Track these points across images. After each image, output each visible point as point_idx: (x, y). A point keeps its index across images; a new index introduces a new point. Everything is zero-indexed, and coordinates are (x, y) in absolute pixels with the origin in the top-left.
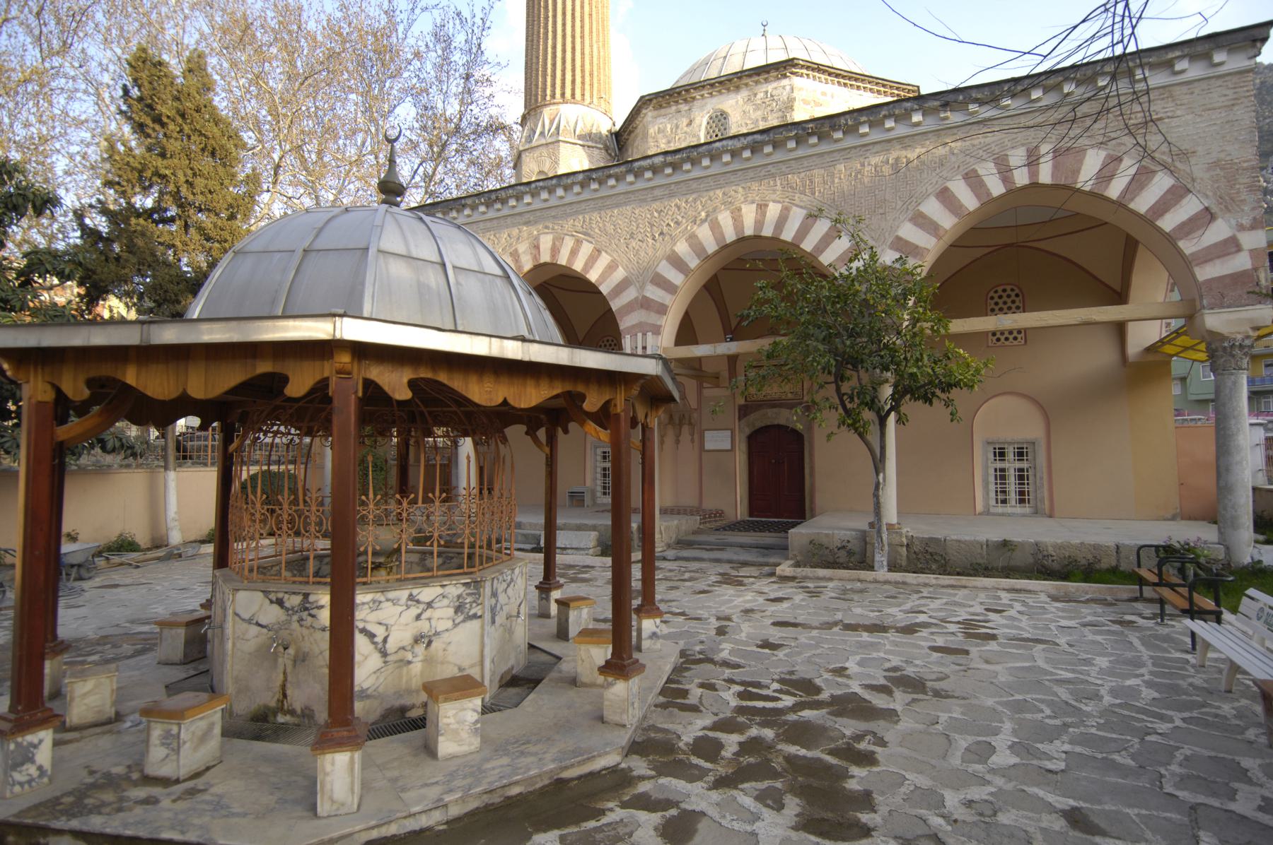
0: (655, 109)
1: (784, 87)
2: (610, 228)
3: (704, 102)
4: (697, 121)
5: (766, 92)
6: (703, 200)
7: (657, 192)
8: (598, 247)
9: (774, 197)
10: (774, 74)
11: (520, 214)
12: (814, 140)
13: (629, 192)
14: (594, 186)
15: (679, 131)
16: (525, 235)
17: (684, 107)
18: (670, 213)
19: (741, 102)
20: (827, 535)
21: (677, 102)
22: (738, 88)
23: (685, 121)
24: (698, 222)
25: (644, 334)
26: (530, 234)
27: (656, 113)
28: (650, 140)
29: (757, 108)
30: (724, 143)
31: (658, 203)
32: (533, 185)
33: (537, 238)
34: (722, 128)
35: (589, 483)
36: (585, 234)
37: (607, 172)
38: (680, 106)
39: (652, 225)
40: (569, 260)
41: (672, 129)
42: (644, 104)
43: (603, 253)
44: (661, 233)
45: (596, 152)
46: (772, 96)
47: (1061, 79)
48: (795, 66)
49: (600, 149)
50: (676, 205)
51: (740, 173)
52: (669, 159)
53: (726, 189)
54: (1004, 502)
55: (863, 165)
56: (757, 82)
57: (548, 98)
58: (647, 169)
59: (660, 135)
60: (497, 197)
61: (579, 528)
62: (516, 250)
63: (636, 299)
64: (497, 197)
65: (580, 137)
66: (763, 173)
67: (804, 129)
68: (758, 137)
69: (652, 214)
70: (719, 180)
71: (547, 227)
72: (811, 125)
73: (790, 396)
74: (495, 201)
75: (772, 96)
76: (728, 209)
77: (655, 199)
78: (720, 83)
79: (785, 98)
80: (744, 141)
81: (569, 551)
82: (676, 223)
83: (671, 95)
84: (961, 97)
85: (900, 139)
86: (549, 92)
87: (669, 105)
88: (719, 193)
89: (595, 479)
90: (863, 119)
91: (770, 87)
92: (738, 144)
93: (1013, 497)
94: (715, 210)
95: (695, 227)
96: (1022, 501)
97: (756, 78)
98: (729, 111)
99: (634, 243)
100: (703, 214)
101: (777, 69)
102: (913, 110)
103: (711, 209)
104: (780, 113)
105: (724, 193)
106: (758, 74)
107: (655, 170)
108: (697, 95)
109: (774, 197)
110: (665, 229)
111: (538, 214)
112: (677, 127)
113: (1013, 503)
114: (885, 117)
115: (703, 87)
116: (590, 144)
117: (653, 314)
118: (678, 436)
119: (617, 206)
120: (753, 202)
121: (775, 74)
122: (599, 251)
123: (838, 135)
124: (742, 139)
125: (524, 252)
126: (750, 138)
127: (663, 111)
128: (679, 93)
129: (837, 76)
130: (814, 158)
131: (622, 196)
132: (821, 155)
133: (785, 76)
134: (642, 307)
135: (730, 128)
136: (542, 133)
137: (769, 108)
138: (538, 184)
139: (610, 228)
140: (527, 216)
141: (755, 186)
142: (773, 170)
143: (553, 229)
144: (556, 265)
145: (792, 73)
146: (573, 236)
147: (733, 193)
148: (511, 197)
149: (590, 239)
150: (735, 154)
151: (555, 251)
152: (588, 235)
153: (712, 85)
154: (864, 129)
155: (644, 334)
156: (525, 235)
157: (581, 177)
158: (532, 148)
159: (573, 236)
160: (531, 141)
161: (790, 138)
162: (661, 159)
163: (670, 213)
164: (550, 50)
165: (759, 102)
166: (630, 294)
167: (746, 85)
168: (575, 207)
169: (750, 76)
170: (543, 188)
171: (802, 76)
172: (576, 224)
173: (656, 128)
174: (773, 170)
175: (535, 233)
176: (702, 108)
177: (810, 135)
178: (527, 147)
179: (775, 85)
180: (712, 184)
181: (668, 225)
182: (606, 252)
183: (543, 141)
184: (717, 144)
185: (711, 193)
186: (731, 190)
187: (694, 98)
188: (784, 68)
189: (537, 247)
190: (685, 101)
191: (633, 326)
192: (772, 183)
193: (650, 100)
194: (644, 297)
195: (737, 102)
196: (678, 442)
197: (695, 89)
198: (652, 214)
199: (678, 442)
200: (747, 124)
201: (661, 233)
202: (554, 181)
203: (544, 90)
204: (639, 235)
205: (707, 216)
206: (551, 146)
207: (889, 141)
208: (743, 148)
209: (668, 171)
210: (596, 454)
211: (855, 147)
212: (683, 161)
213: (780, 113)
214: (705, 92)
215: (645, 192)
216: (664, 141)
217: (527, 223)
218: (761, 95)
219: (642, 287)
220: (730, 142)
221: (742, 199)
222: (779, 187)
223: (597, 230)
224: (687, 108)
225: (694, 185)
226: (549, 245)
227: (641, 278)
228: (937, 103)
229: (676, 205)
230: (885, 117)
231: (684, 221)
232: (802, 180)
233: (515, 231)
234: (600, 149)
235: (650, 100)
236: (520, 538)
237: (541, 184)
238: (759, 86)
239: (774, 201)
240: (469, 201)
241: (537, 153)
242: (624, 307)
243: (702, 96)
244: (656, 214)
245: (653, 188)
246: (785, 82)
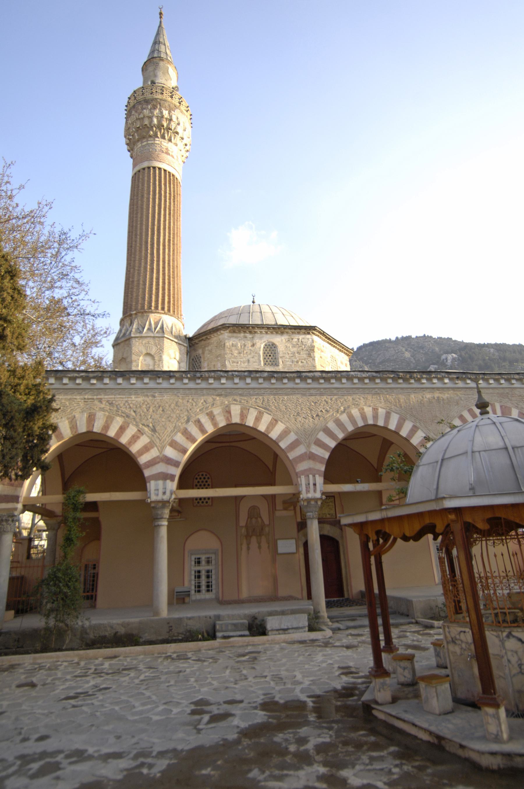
0: (230, 332)
1: (308, 339)
2: (283, 408)
3: (262, 335)
4: (258, 345)
5: (299, 339)
6: (342, 401)
7: (312, 391)
8: (275, 418)
9: (381, 405)
10: (303, 331)
11: (214, 389)
12: (401, 381)
13: (294, 388)
14: (273, 381)
15: (246, 348)
16: (218, 402)
17: (249, 336)
18: (322, 405)
19: (284, 341)
20: (434, 600)
21: (245, 332)
22: (282, 333)
23: (249, 344)
24: (340, 412)
25: (314, 476)
26: (222, 403)
27: (230, 335)
28: (227, 349)
29: (294, 346)
30: (356, 373)
31: (313, 397)
32: (230, 373)
33: (228, 406)
34: (273, 352)
35: (186, 584)
36: (265, 408)
37: (284, 375)
38: (246, 334)
39: (311, 410)
40: (254, 423)
41: (241, 346)
42: (224, 328)
43: (279, 422)
44: (317, 415)
45: (183, 348)
46: (302, 342)
47: (500, 377)
48: (315, 330)
49: (185, 346)
50: (325, 400)
51: (361, 390)
52: (324, 375)
53: (354, 396)
54: (199, 591)
55: (423, 397)
56: (293, 333)
57: (153, 308)
58: (309, 378)
59: (233, 348)
60: (201, 376)
61: (293, 612)
62: (211, 412)
63: (305, 453)
64: (201, 376)
65: (176, 337)
66: (373, 392)
67: (398, 375)
68: (374, 374)
69: (310, 403)
70: (349, 391)
71: (235, 400)
72: (401, 374)
73: (328, 516)
74: (199, 378)
75: (302, 342)
76: (357, 408)
77: (311, 395)
78: (273, 328)
79: (309, 344)
80: (367, 375)
81: (290, 631)
82: (326, 411)
83: (242, 327)
84: (464, 376)
85: (438, 389)
86: (153, 304)
87: (240, 332)
88: (350, 398)
89: (190, 581)
90: (424, 376)
91: (301, 337)
92: (364, 375)
93: (203, 588)
94: (349, 407)
95: (338, 415)
96: (208, 591)
97: (293, 331)
98: (277, 344)
99: (300, 419)
100: (342, 408)
101: (305, 329)
102: (445, 377)
103: (346, 406)
104: (307, 352)
105: (353, 399)
106: (295, 329)
107: (314, 379)
108: (258, 331)
109: (381, 405)
110: (320, 414)
111: (228, 391)
112: (245, 346)
113: (204, 592)
114: (434, 377)
115: (263, 328)
116: (180, 342)
117: (317, 463)
118: (248, 544)
119: (287, 394)
120: (370, 406)
121: (304, 331)
122: (276, 421)
123: (412, 381)
124: (366, 373)
125: (218, 414)
126: (369, 373)
127: (235, 335)
128: (248, 328)
129: (329, 339)
130: (399, 389)
131: (289, 390)
132: (402, 388)
133: (309, 333)
134: (310, 458)
135: (278, 353)
136: (149, 329)
137: (301, 348)
138: (234, 373)
139: (283, 408)
140: (219, 391)
141: (370, 397)
142: (379, 392)
143: (240, 402)
144: (245, 425)
145: (313, 333)
146: (256, 408)
147: (357, 399)
148: (212, 377)
149: (269, 412)
150: (361, 379)
151: (243, 416)
152: (268, 410)
153: (268, 328)
154: (424, 381)
155: (314, 476)
156: (218, 402)
157: (266, 374)
158: (142, 337)
159: (256, 408)
160: (141, 332)
161: (390, 378)
162: (319, 374)
163: (322, 405)
164: (154, 280)
165: (295, 343)
166: (300, 450)
167: (287, 332)
168: (257, 391)
169: (290, 329)
170: (237, 376)
171: (316, 335)
172: (258, 401)
173: (231, 343)
174: (379, 392)
175: (226, 402)
176: (261, 338)
177: (399, 378)
178: (138, 335)
179: (303, 336)
180: (345, 392)
181: (321, 411)
182: (282, 422)
183: (151, 334)
184: (352, 373)
185: (346, 397)
186: (356, 397)
187: (255, 332)
188: (309, 329)
189: (229, 412)
190: (250, 332)
191: (305, 470)
192: (378, 398)
193: (229, 327)
194: (311, 452)
195: (282, 340)
196: (248, 548)
197: (258, 327)
198: (310, 403)
199: (248, 548)
200: (288, 354)
201: (317, 415)
202: (246, 374)
203: (150, 303)
204: (303, 414)
205: (345, 409)
206: (157, 339)
207: (433, 388)
208: (365, 378)
209: (322, 381)
210: (191, 561)
211: (418, 388)
212: (332, 378)
213: (307, 352)
214: (263, 331)
215: (305, 390)
216: (236, 352)
217: (219, 395)
218: (295, 340)
219: (309, 446)
220: (359, 373)
221: (364, 404)
222: (382, 401)
223: (273, 407)
224: (251, 336)
225: (335, 391)
226: (239, 412)
227: (307, 441)
228: (455, 376)
229: (325, 400)
230: (434, 377)
231: (331, 410)
232: (394, 399)
233: (210, 399)
234: (185, 346)
235: (229, 327)
236: (230, 628)
237: (236, 373)
238: (294, 335)
239: (381, 408)
240: (177, 375)
241: (145, 341)
242: (297, 457)
243: (261, 332)
244: (313, 404)
245: (309, 389)
246: (308, 336)
